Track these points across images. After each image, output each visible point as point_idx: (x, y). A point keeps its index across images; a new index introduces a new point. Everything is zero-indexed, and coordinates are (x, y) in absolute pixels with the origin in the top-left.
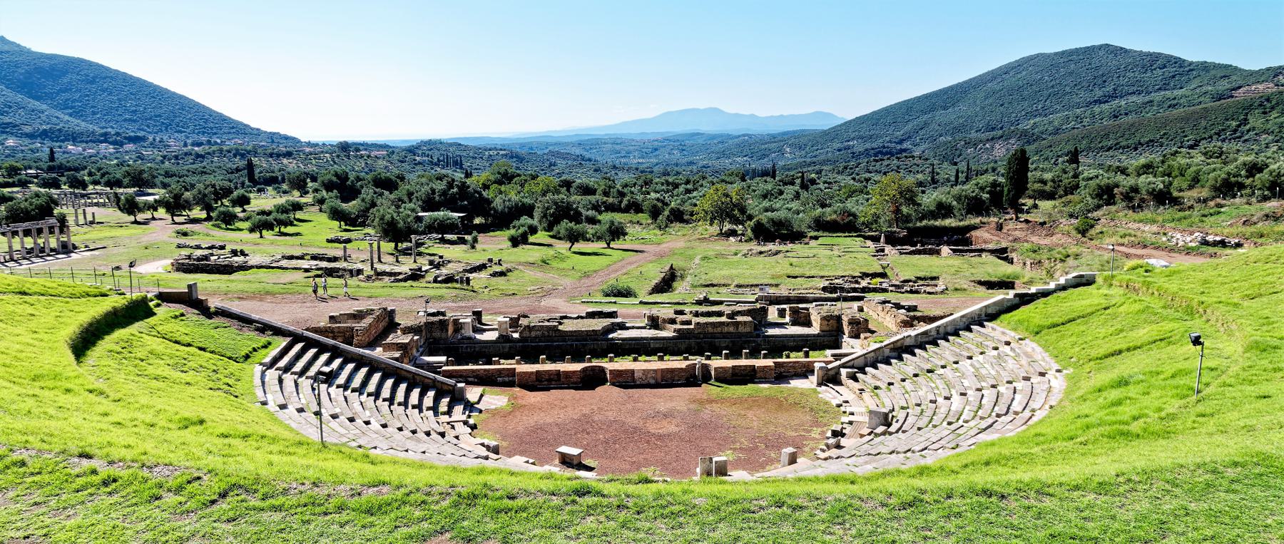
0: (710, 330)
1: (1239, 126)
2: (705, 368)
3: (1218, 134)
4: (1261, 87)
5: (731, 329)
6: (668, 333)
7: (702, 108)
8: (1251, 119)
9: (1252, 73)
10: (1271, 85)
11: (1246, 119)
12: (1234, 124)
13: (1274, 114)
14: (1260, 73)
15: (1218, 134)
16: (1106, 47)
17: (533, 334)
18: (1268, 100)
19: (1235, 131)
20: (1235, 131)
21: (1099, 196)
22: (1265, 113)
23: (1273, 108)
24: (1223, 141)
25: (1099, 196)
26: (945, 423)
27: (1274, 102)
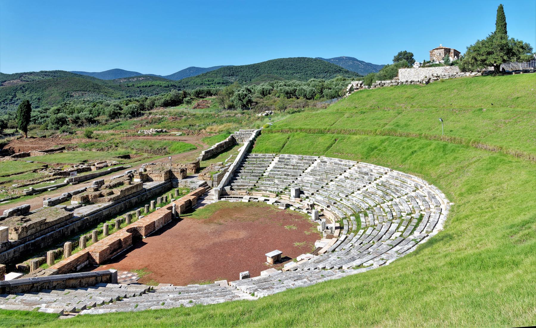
0: (127, 194)
1: (13, 98)
2: (134, 232)
3: (4, 101)
4: (15, 81)
5: (134, 190)
6: (104, 204)
7: (11, 73)
8: (17, 95)
9: (9, 75)
10: (19, 81)
11: (15, 95)
12: (10, 97)
13: (27, 93)
14: (13, 75)
15: (4, 101)
16: (190, 69)
17: (29, 233)
18: (24, 87)
19: (11, 100)
20: (11, 100)
21: (57, 123)
22: (23, 92)
23: (26, 90)
24: (7, 104)
25: (57, 123)
26: (188, 300)
27: (26, 88)
